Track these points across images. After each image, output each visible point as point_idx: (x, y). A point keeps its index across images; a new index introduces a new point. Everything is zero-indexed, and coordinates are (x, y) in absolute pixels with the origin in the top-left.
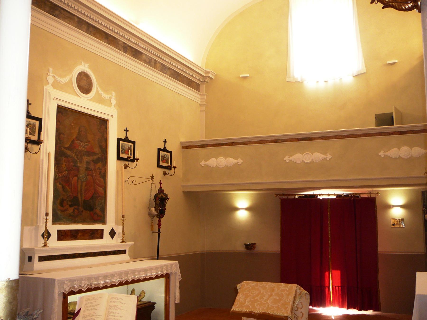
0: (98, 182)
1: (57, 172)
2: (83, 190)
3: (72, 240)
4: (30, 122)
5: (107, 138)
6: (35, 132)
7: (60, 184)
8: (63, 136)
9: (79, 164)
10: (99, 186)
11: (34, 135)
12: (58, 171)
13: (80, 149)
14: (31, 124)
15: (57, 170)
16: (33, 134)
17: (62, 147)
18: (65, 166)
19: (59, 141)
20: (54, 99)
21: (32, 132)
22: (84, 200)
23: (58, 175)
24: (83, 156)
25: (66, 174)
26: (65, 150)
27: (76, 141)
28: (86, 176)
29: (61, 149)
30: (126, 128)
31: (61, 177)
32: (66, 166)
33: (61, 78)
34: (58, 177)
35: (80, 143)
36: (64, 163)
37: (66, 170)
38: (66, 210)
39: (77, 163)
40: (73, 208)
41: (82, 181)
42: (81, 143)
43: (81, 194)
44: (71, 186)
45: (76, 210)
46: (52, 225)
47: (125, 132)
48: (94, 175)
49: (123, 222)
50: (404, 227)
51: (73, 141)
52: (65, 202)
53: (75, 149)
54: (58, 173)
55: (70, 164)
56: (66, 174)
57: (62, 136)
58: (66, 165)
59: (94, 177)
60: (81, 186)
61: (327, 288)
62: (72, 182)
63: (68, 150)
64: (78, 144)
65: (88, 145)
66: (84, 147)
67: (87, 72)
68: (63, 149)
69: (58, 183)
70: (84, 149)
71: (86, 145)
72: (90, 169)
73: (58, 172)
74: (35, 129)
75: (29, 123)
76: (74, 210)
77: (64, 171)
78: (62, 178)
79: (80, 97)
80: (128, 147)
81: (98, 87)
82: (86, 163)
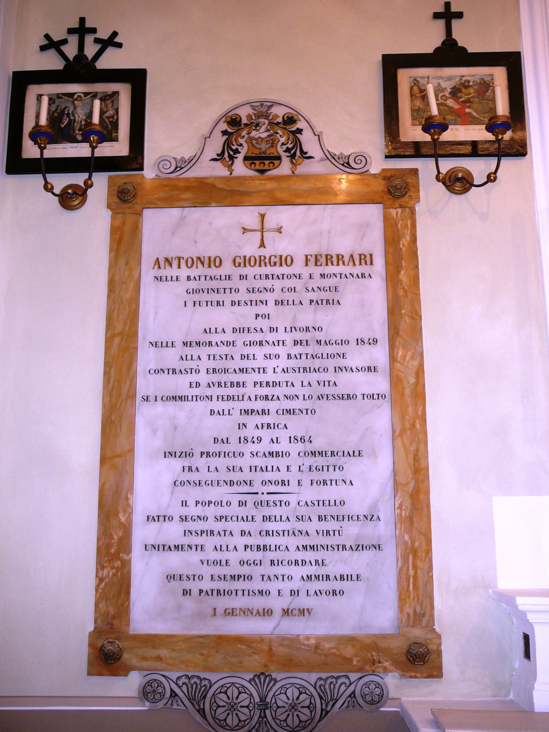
4: (464, 79)
6: (115, 125)
14: (471, 84)
75: (462, 81)
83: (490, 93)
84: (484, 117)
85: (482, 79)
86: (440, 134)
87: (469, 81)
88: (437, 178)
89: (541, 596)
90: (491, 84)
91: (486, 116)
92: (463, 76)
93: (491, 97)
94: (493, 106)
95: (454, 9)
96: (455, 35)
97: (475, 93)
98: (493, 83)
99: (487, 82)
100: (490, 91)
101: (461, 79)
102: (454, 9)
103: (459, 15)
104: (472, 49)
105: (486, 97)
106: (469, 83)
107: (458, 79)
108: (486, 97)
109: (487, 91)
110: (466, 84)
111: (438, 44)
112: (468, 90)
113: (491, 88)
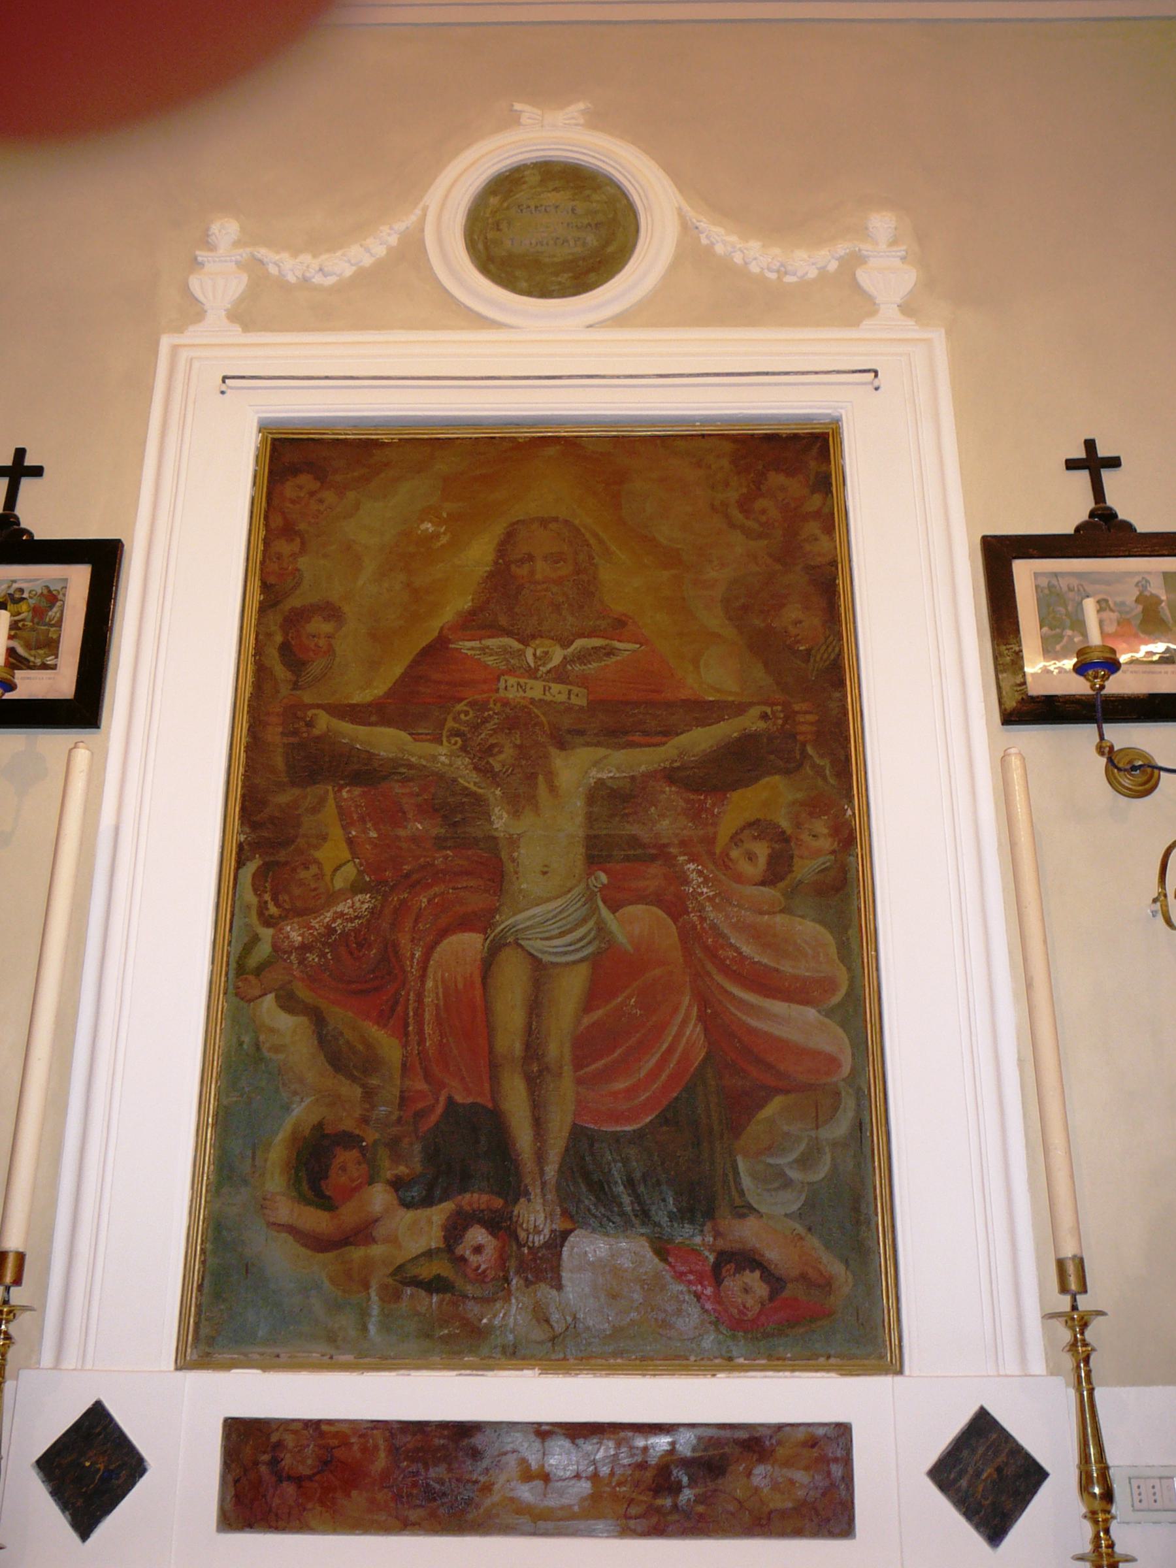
0: (746, 950)
1: (262, 908)
2: (558, 1048)
3: (405, 1526)
4: (15, 586)
5: (834, 563)
6: (52, 646)
7: (288, 1003)
8: (327, 627)
9: (498, 824)
10: (787, 995)
11: (50, 660)
12: (275, 899)
13: (511, 695)
14: (25, 595)
15: (267, 897)
16: (38, 661)
17: (319, 706)
18: (347, 855)
19: (280, 671)
20: (223, 393)
21: (28, 647)
22: (578, 1133)
23: (267, 933)
24: (553, 751)
25: (351, 920)
26: (348, 730)
27: (467, 646)
28: (595, 910)
29: (310, 724)
30: (37, 471)
31: (304, 948)
32: (354, 855)
33: (315, 256)
34: (276, 947)
35: (521, 654)
36: (336, 832)
37: (356, 888)
38: (362, 1233)
39: (487, 816)
40: (439, 1214)
41: (546, 958)
42: (529, 652)
43: (534, 1083)
44: (419, 1015)
45: (478, 1235)
46: (183, 1364)
47: (1083, 476)
48: (695, 895)
49: (1073, 1345)
50: (1074, 642)
51: (437, 650)
52: (346, 1157)
53: (460, 707)
54: (268, 922)
55: (402, 833)
56: (351, 920)
57: (319, 626)
58: (350, 842)
59: (694, 917)
60: (535, 1007)
61: (498, 1203)
62: (430, 984)
63: (385, 721)
64: (490, 660)
65: (610, 652)
66: (560, 675)
67: (508, 162)
68: (324, 722)
69: (270, 999)
70: (558, 692)
71: (583, 657)
72: (643, 846)
73: (273, 910)
74: (61, 620)
75: (11, 591)
76: (455, 1230)
77: (333, 897)
78: (312, 958)
79: (511, 327)
80: (1136, 593)
81: (690, 213)
82: (591, 799)
83: (56, 613)
84: (35, 657)
85: (47, 587)
86: (1105, 678)
87: (21, 590)
88: (1006, 750)
89: (621, 1424)
90: (60, 597)
91: (39, 654)
92: (14, 581)
93: (56, 619)
94: (55, 637)
95: (1102, 452)
96: (1111, 501)
97: (29, 611)
98: (64, 595)
99: (54, 592)
100: (55, 609)
101: (9, 587)
102: (1102, 452)
103: (1114, 463)
104: (1143, 526)
105: (47, 620)
106: (23, 594)
107: (4, 586)
108: (47, 620)
109: (51, 608)
110: (17, 596)
111: (1083, 516)
112: (19, 605)
113: (59, 604)
